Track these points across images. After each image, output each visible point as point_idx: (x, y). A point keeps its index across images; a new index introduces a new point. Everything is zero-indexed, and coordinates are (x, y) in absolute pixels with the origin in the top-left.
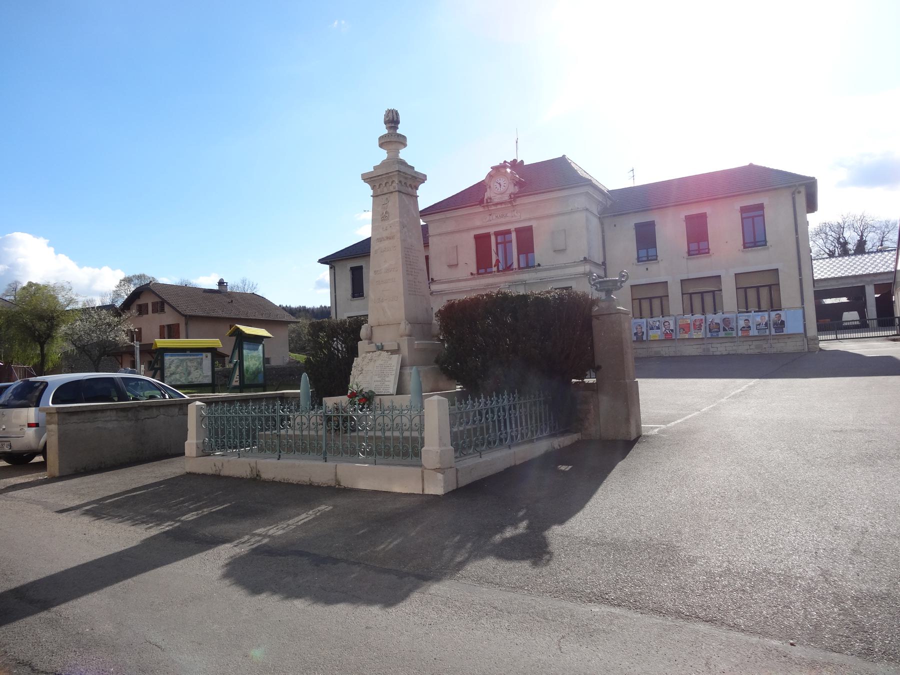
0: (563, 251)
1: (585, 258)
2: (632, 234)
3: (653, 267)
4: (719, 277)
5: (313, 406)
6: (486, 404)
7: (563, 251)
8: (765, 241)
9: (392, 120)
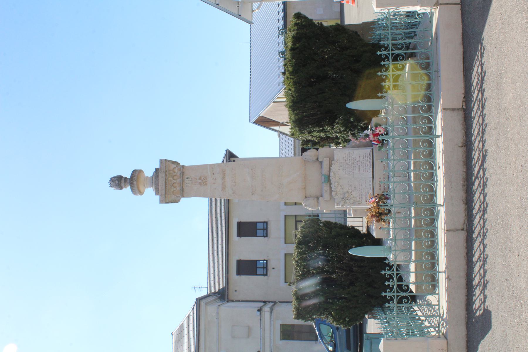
0: (249, 329)
1: (259, 310)
3: (271, 265)
4: (285, 254)
5: (381, 97)
6: (386, 48)
7: (249, 329)
8: (264, 222)
9: (118, 182)
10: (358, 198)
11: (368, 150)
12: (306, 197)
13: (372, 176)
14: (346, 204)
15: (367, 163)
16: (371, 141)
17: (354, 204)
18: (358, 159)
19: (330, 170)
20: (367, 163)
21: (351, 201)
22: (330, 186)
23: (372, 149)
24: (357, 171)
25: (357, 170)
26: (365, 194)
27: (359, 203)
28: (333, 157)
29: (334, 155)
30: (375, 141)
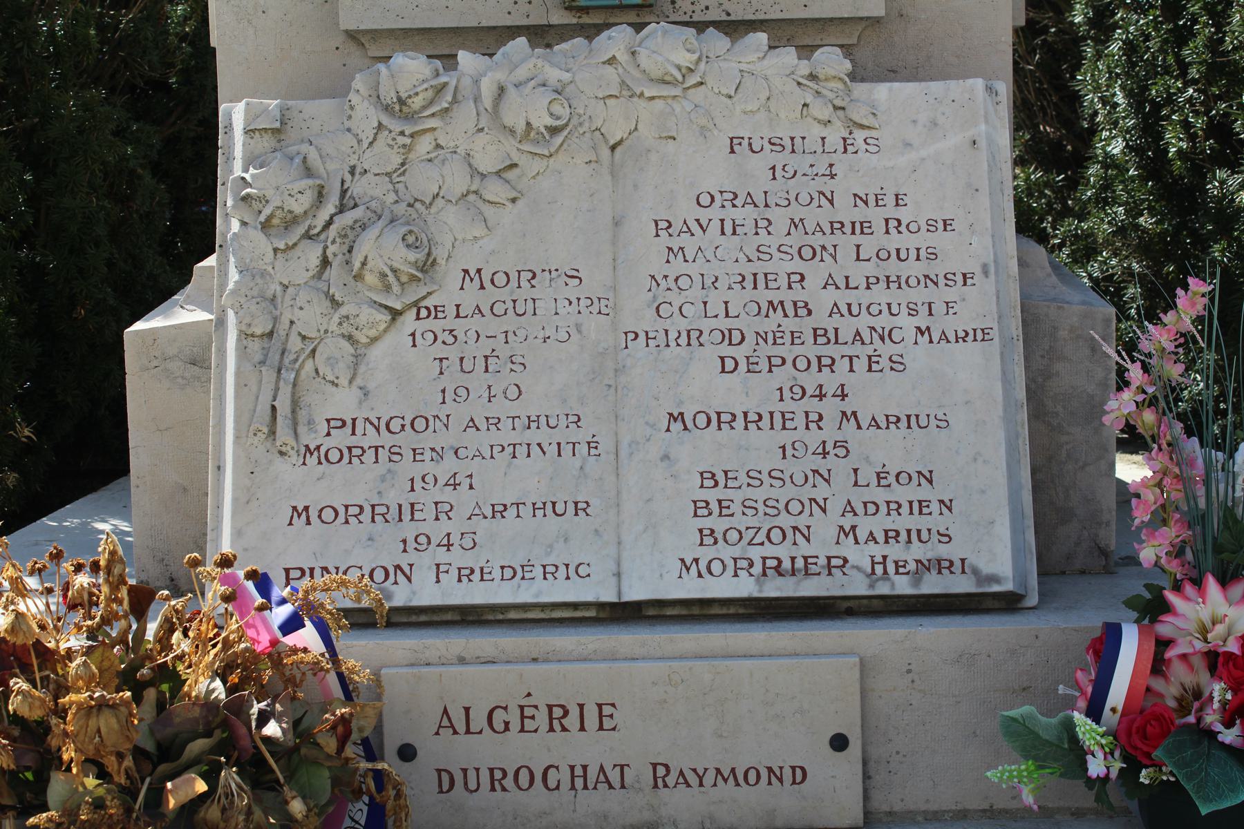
10: (343, 402)
11: (994, 548)
13: (634, 593)
14: (261, 244)
15: (824, 529)
16: (1153, 608)
17: (272, 348)
18: (874, 395)
19: (734, 28)
20: (824, 529)
21: (309, 315)
22: (512, 32)
23: (1009, 603)
24: (704, 383)
25: (737, 394)
26: (395, 496)
27: (277, 423)
28: (892, 74)
29: (943, 75)
30: (1158, 666)
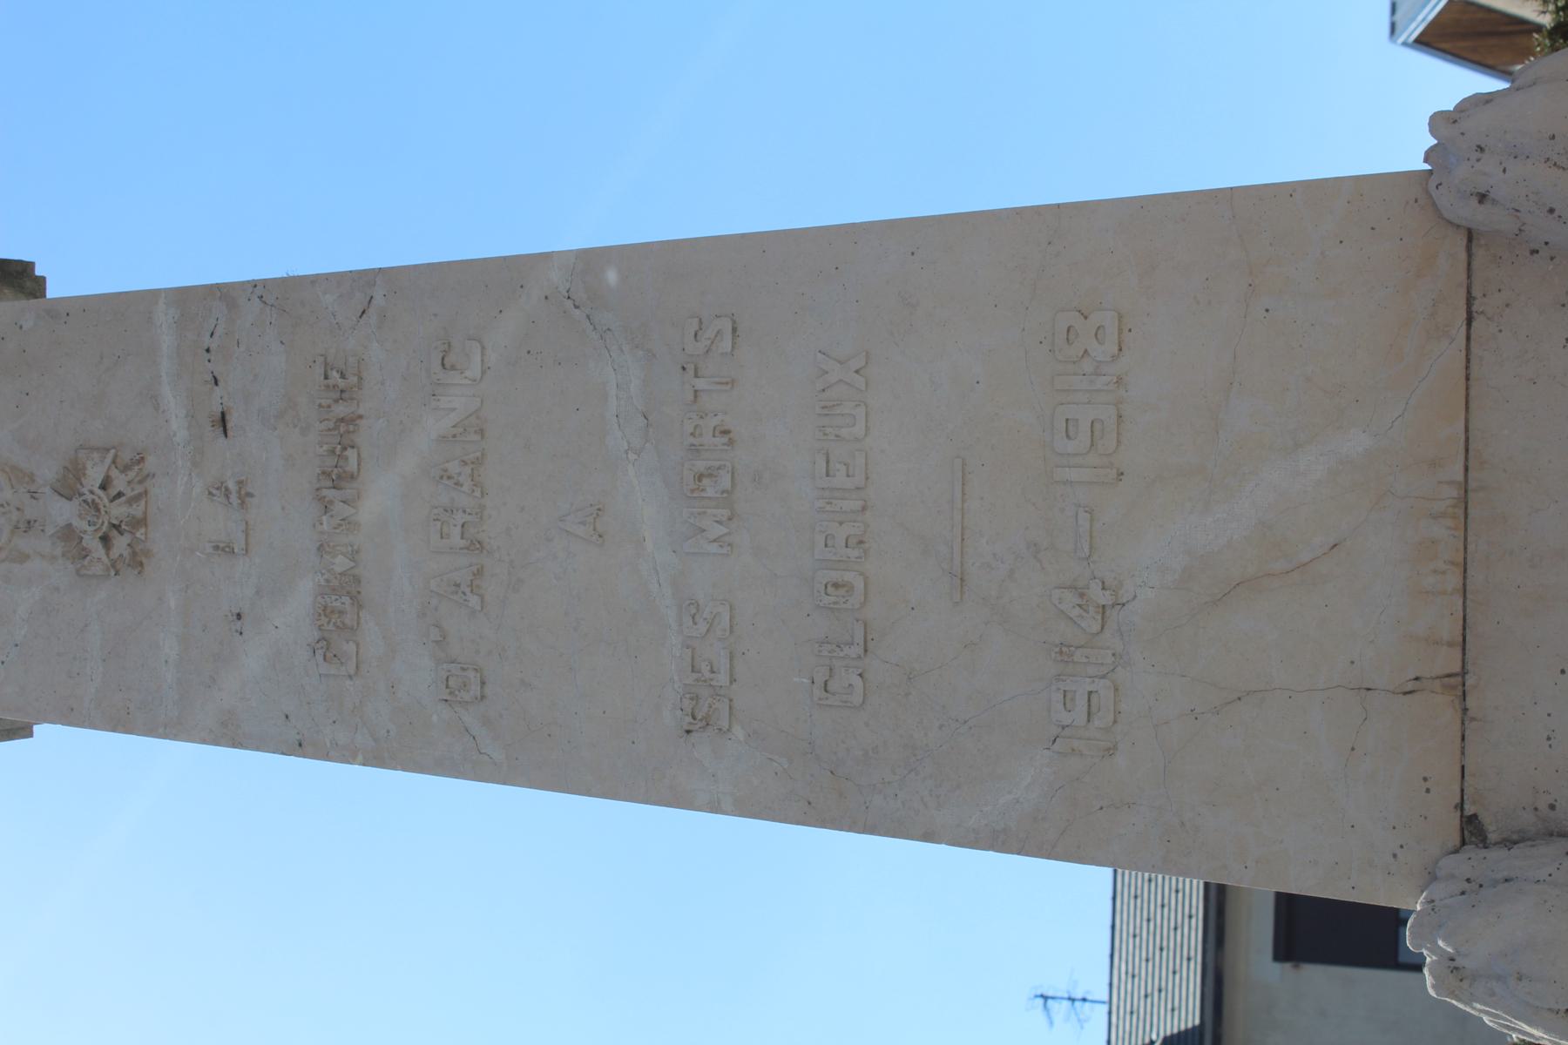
2: (1319, 977)
12: (1472, 831)
